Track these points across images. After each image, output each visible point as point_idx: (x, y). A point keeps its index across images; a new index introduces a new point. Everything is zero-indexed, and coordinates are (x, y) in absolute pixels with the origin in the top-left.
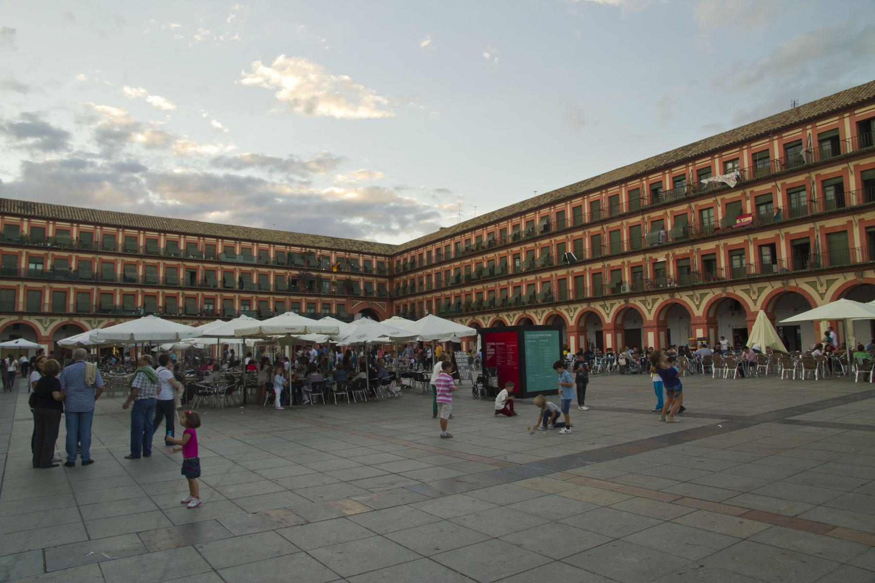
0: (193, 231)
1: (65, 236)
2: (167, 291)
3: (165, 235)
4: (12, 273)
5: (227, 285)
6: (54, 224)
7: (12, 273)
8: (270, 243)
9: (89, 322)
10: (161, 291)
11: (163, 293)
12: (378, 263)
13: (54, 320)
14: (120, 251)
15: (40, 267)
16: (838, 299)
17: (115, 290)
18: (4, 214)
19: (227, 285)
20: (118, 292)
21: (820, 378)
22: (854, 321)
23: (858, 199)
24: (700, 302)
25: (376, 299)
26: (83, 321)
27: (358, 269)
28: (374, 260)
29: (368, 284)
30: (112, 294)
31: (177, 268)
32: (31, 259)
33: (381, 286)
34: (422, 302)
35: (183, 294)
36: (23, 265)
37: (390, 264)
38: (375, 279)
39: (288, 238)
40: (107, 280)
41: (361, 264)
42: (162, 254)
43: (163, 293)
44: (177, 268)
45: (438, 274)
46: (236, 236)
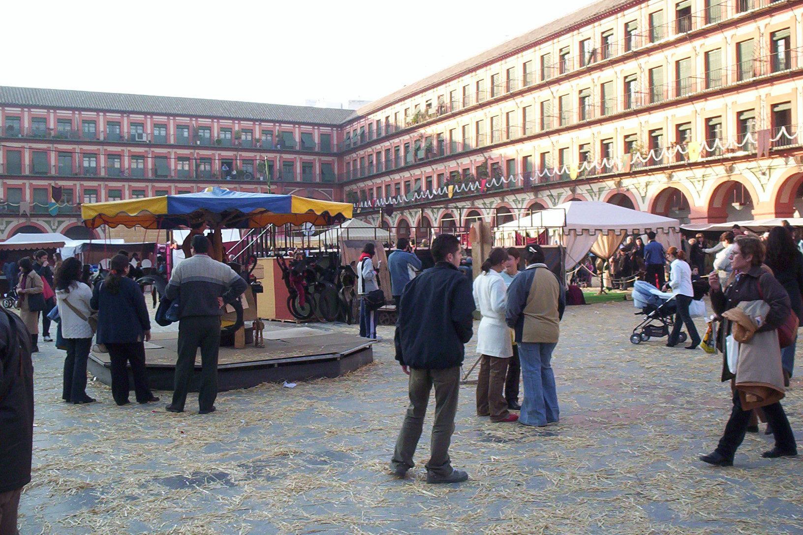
2: (35, 182)
3: (55, 113)
5: (159, 173)
6: (29, 111)
8: (168, 115)
9: (48, 223)
10: (27, 182)
11: (31, 184)
12: (322, 135)
13: (63, 222)
15: (208, 168)
16: (14, 235)
17: (24, 184)
18: (4, 105)
20: (126, 187)
23: (486, 347)
26: (41, 222)
27: (312, 148)
29: (307, 167)
30: (21, 189)
31: (46, 152)
33: (326, 166)
34: (372, 189)
37: (339, 137)
38: (317, 158)
40: (41, 173)
41: (317, 140)
42: (102, 138)
43: (31, 184)
44: (46, 152)
45: (388, 151)
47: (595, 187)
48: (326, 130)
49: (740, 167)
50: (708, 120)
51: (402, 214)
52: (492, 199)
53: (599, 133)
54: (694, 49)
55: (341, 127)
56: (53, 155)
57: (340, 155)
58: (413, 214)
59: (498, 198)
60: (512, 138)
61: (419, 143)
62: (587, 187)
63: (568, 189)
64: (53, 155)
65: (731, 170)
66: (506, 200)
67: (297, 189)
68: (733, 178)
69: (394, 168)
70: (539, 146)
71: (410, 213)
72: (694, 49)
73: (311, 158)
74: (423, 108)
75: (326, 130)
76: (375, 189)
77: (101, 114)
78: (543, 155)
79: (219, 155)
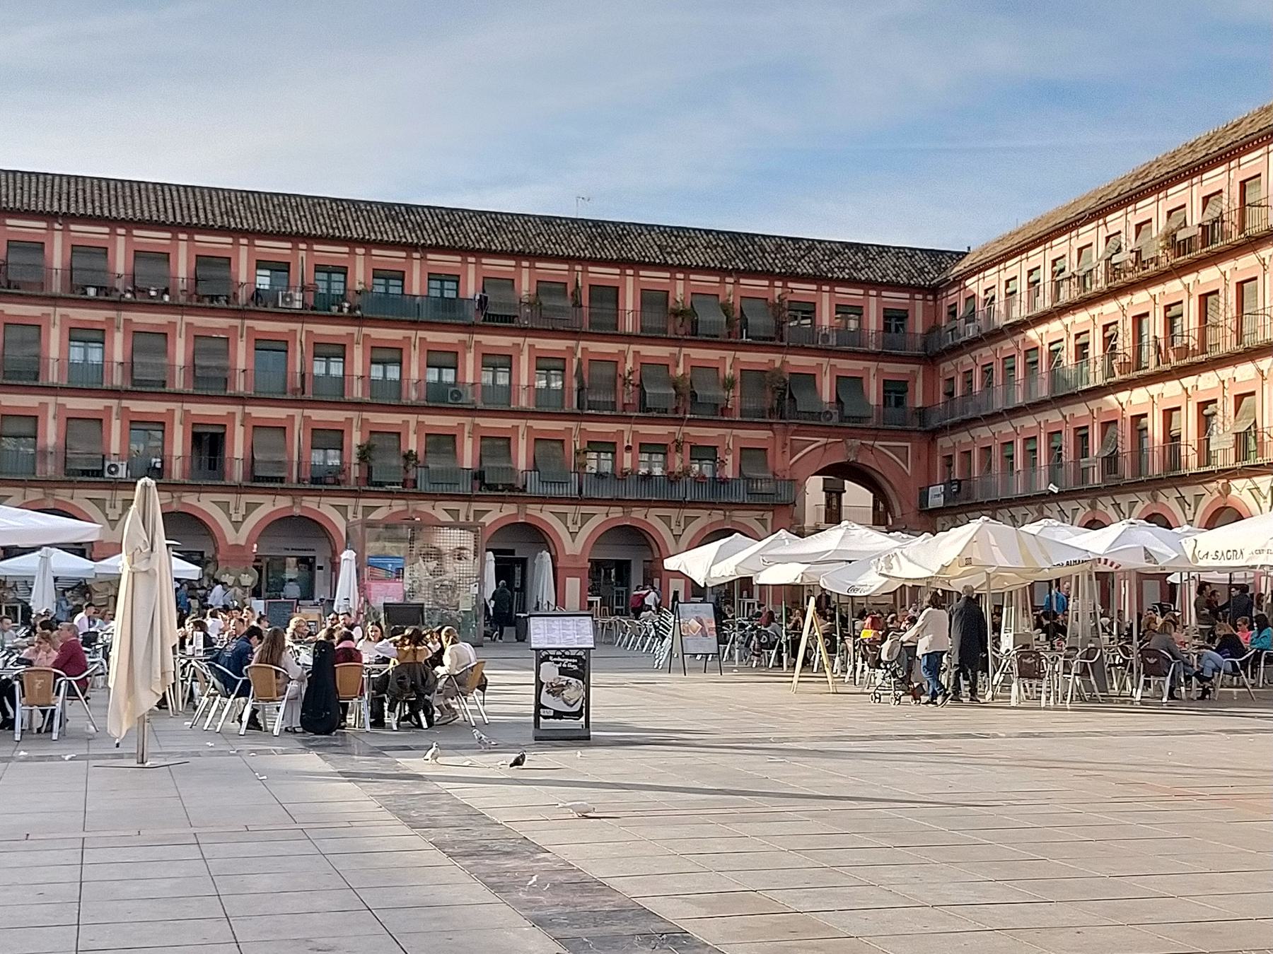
0: (275, 224)
1: (97, 263)
4: (27, 377)
5: (847, 412)
7: (27, 377)
14: (56, 287)
17: (44, 405)
19: (847, 412)
20: (412, 425)
21: (430, 724)
22: (38, 356)
24: (245, 517)
25: (877, 433)
28: (873, 302)
29: (849, 385)
31: (98, 421)
32: (78, 334)
33: (895, 391)
35: (246, 416)
36: (54, 352)
38: (872, 365)
39: (581, 240)
43: (306, 419)
46: (411, 238)
47: (1188, 492)
48: (896, 299)
49: (1237, 484)
52: (1200, 490)
54: (1187, 287)
56: (116, 427)
57: (931, 357)
58: (1125, 507)
64: (116, 427)
66: (1162, 499)
67: (823, 441)
69: (1100, 381)
71: (1181, 499)
72: (1187, 287)
75: (896, 299)
76: (1019, 443)
77: (360, 251)
78: (1168, 414)
79: (636, 353)
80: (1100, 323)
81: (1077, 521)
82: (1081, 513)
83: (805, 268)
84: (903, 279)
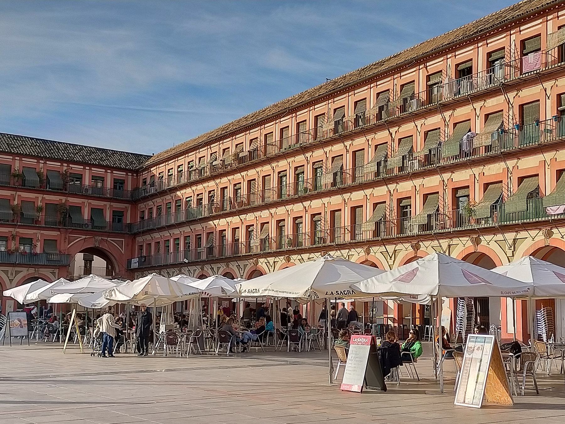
25: (109, 235)
29: (97, 212)
33: (118, 216)
49: (485, 239)
50: (400, 201)
51: (202, 269)
52: (246, 262)
53: (516, 167)
55: (137, 172)
58: (215, 269)
59: (223, 264)
60: (285, 198)
61: (338, 163)
62: (382, 249)
63: (408, 245)
65: (477, 242)
66: (231, 266)
67: (84, 237)
68: (480, 249)
69: (206, 215)
70: (329, 203)
72: (243, 177)
73: (102, 203)
74: (196, 165)
80: (373, 144)
81: (195, 276)
82: (221, 270)
83: (78, 158)
84: (123, 166)
